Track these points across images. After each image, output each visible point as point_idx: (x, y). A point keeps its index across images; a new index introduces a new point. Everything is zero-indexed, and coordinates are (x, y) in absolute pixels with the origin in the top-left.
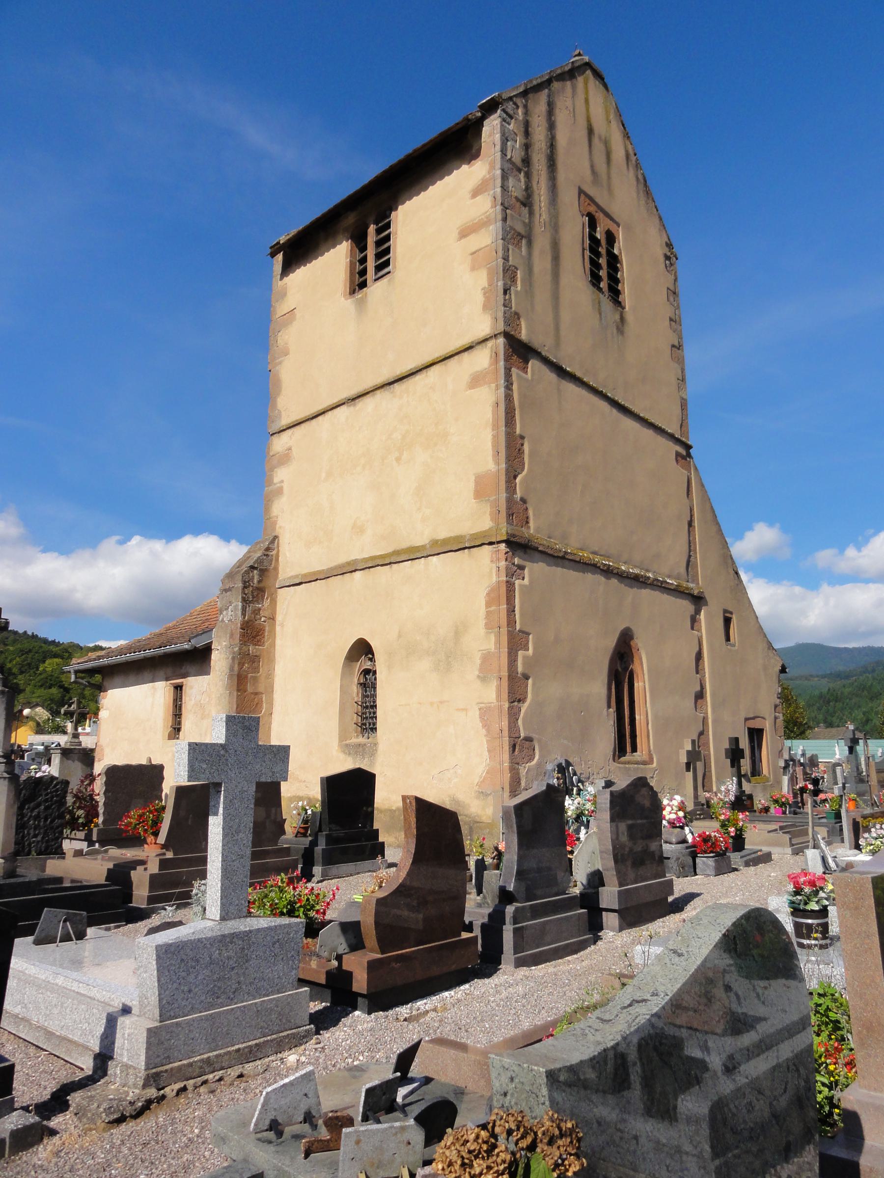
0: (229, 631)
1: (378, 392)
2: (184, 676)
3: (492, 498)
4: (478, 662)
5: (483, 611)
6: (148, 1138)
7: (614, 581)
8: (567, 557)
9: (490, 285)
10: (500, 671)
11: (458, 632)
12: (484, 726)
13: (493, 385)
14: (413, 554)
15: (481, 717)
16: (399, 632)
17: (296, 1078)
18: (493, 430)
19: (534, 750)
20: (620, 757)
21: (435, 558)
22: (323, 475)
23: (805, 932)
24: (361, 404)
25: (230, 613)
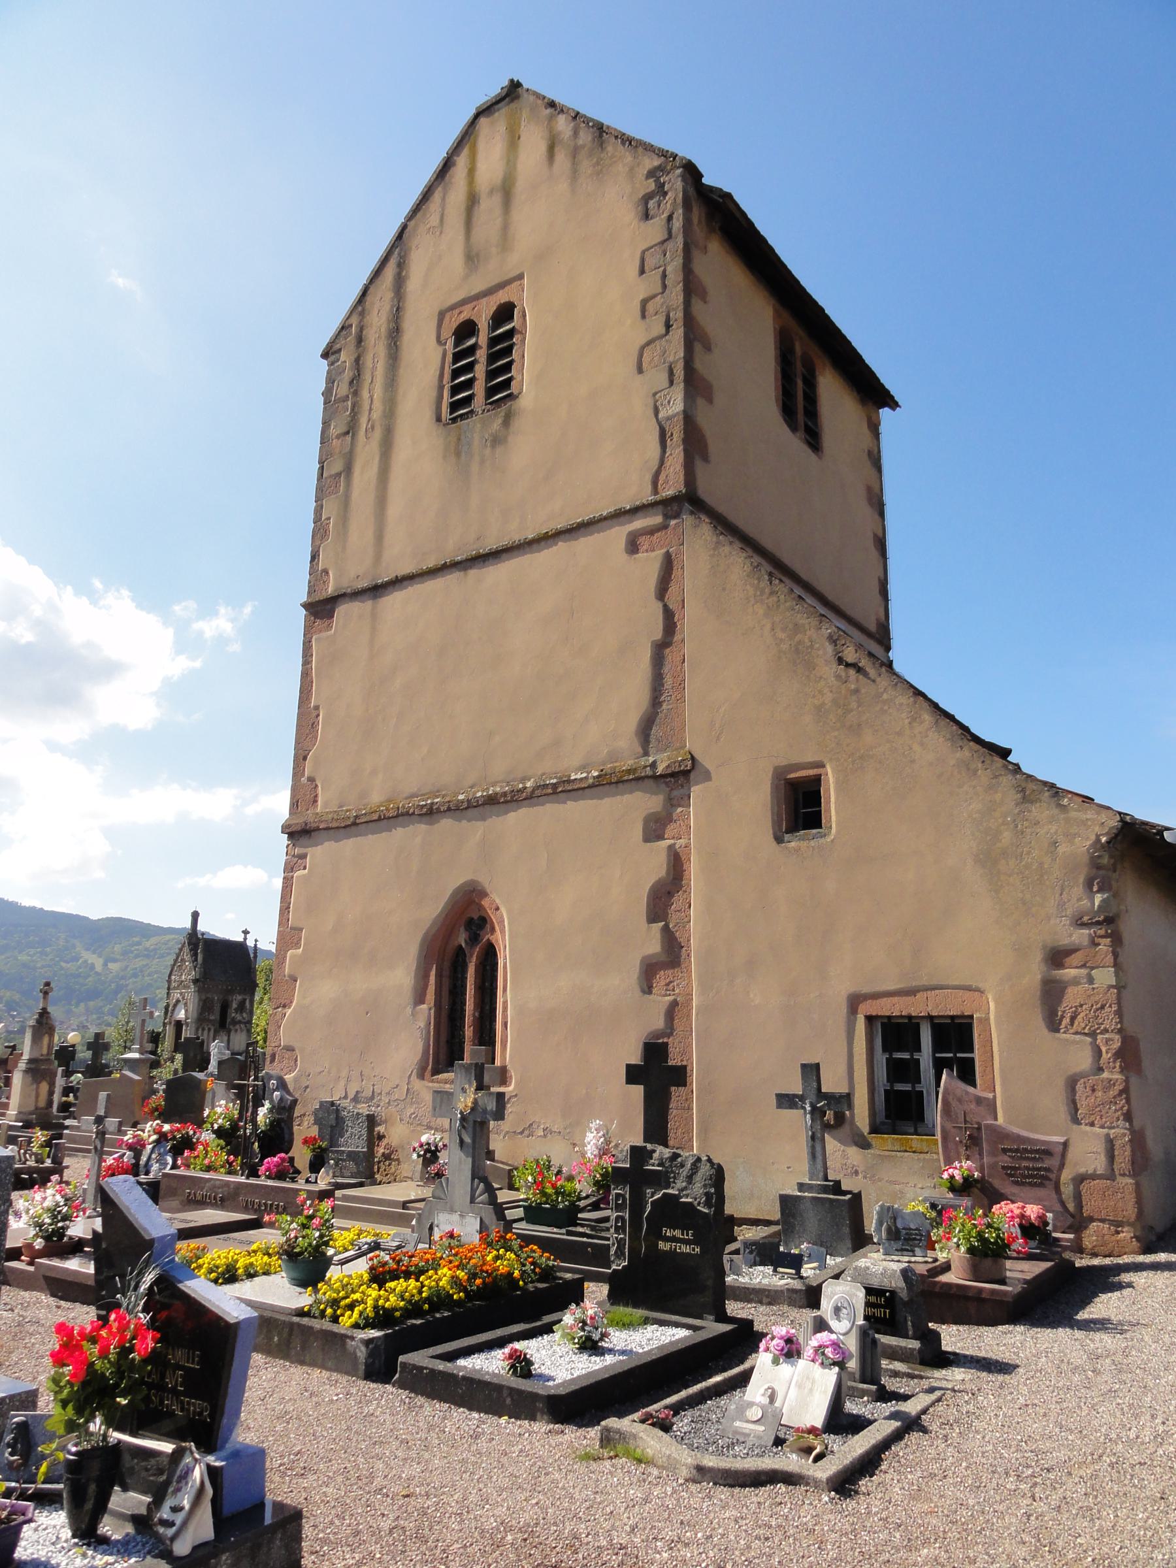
7: (446, 824)
8: (358, 821)
17: (705, 1380)
19: (296, 1061)
20: (436, 1072)
23: (19, 1446)
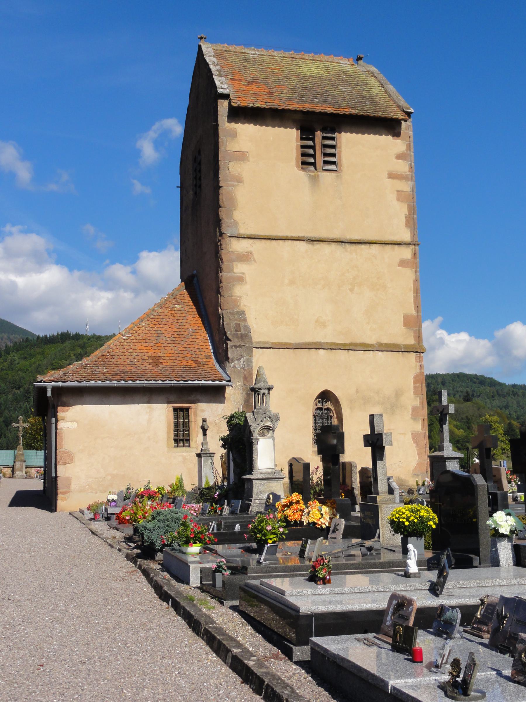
0: (242, 375)
1: (333, 243)
2: (193, 402)
3: (415, 329)
4: (411, 411)
5: (412, 385)
6: (483, 512)
9: (410, 214)
10: (423, 416)
11: (398, 394)
12: (414, 442)
13: (414, 270)
14: (366, 347)
15: (413, 439)
16: (357, 389)
18: (414, 293)
21: (380, 353)
22: (286, 281)
24: (318, 246)
25: (242, 363)
